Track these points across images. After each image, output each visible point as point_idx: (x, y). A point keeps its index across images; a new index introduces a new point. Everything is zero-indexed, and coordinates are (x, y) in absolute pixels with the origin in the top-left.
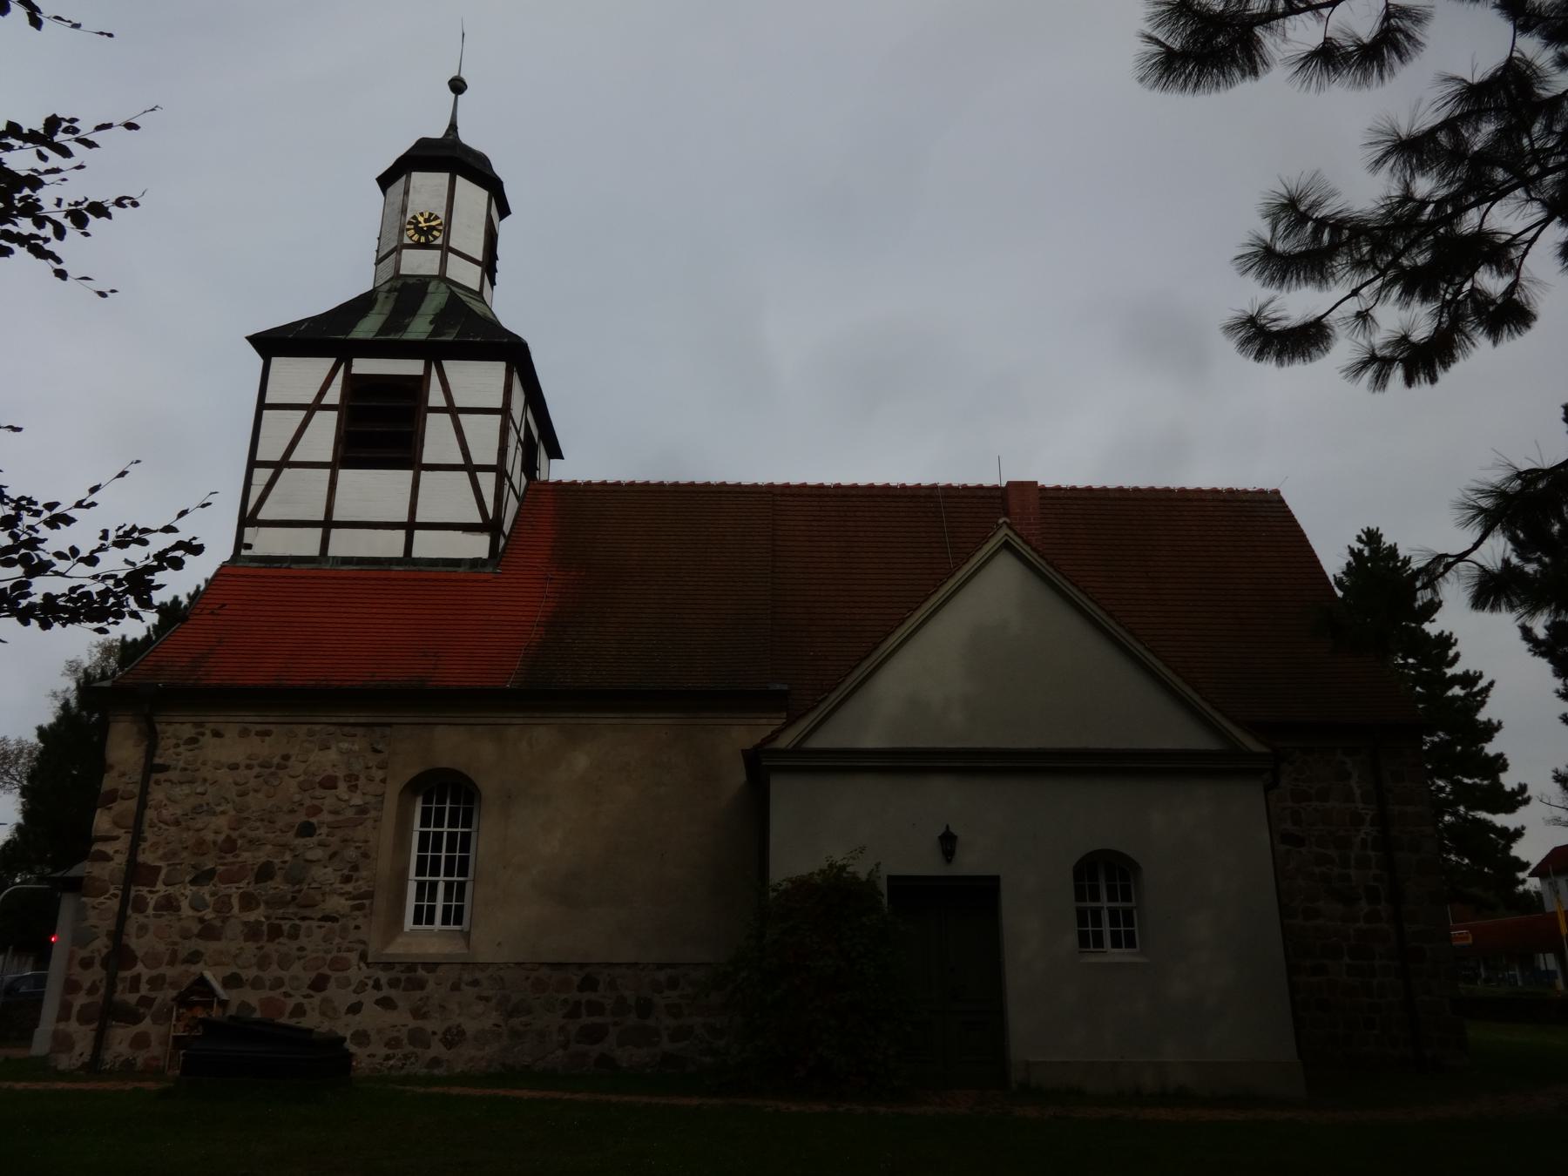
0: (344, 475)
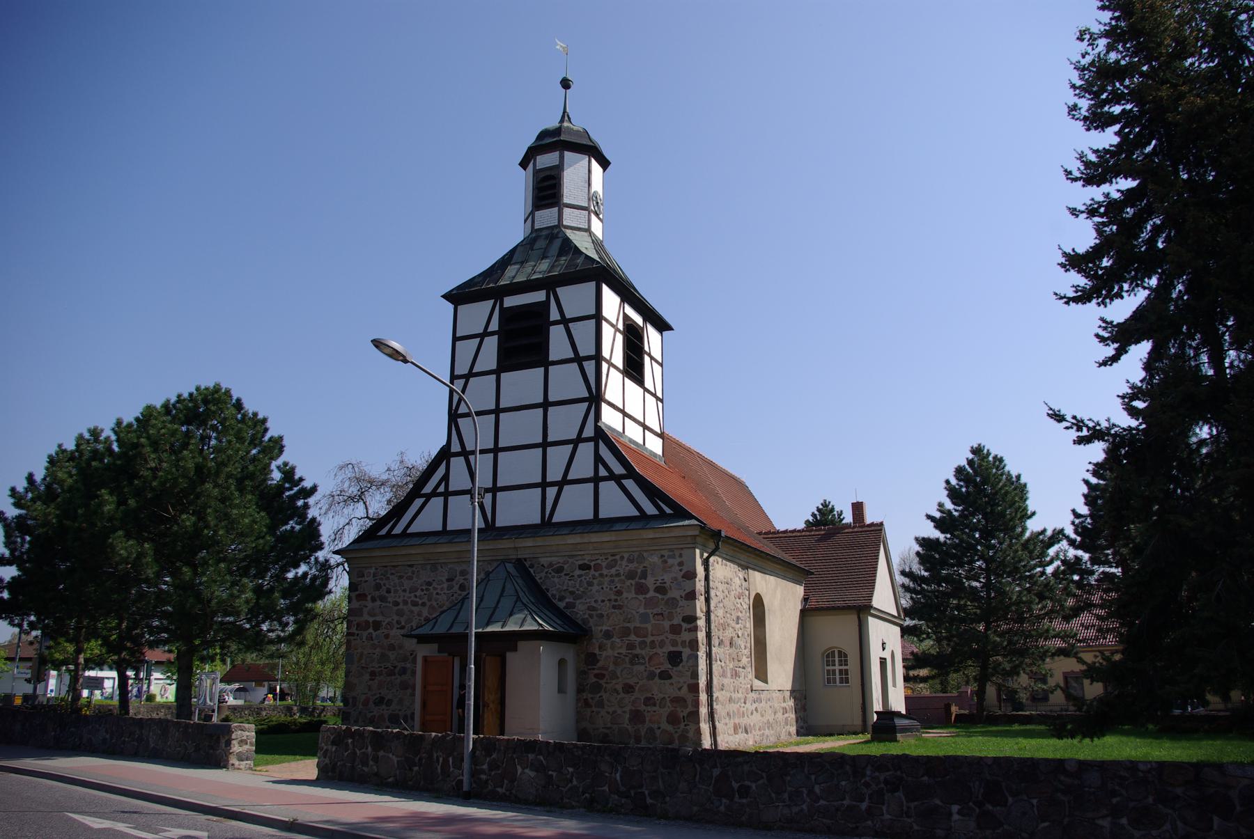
0: (505, 376)
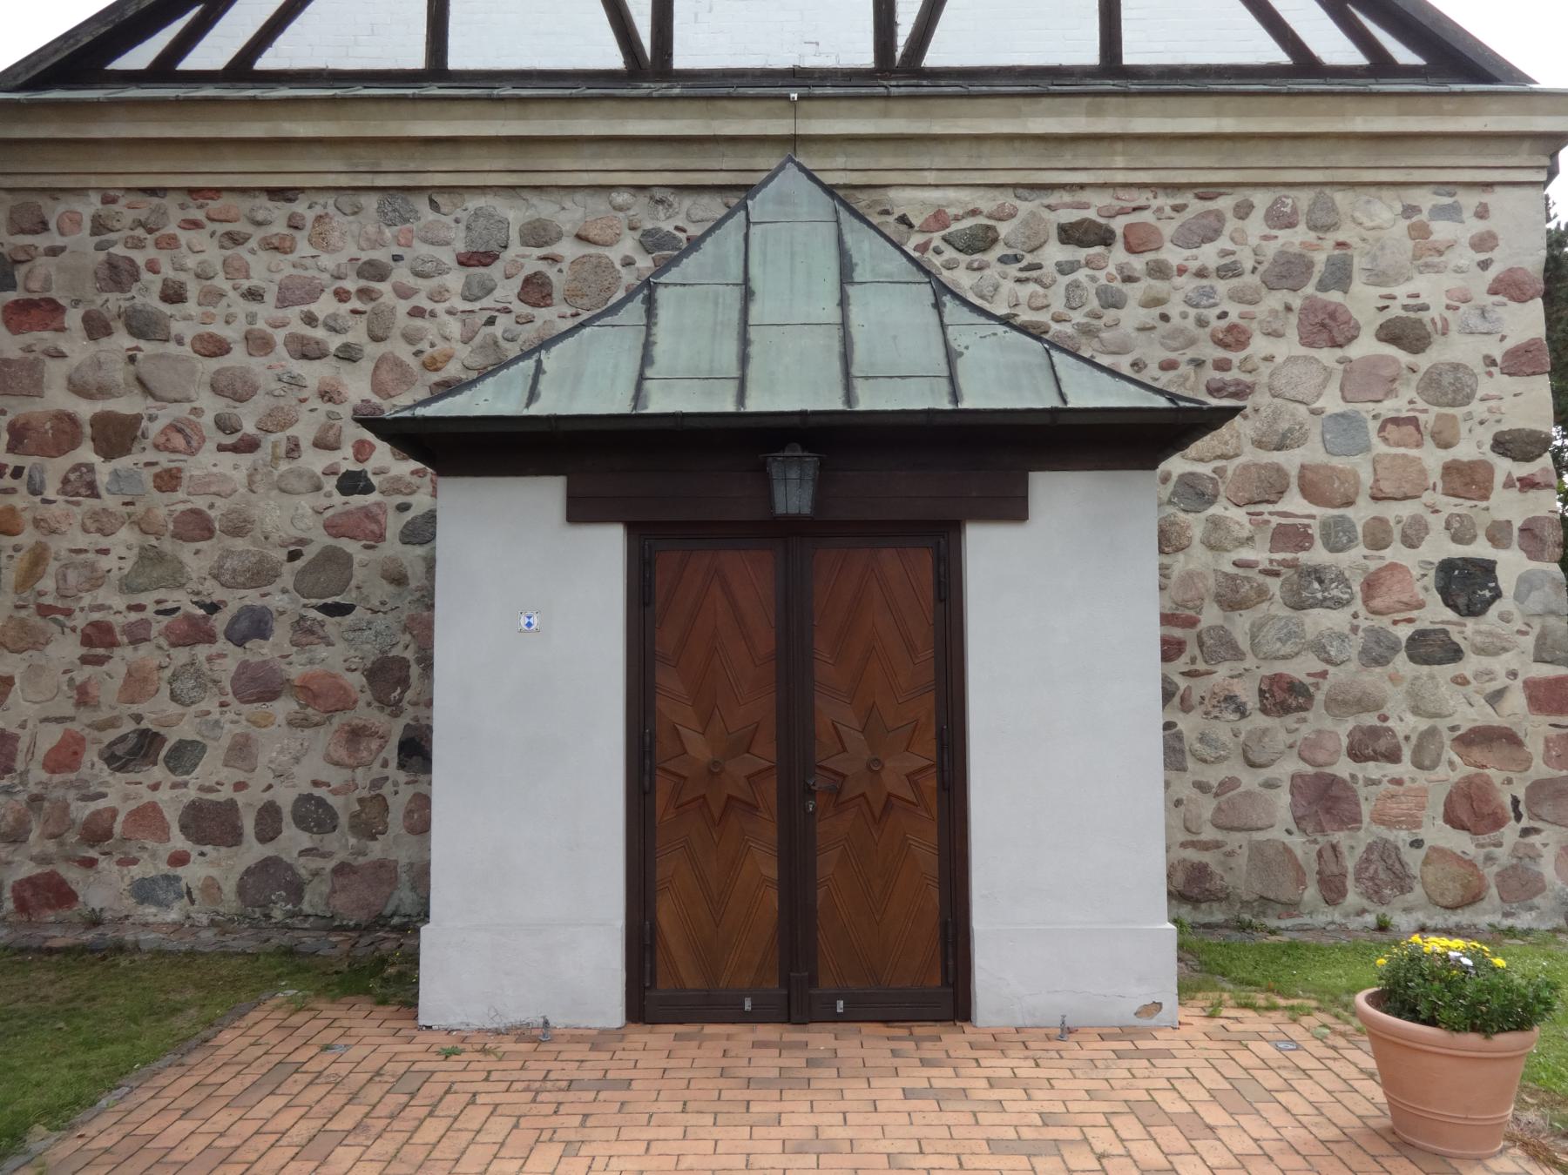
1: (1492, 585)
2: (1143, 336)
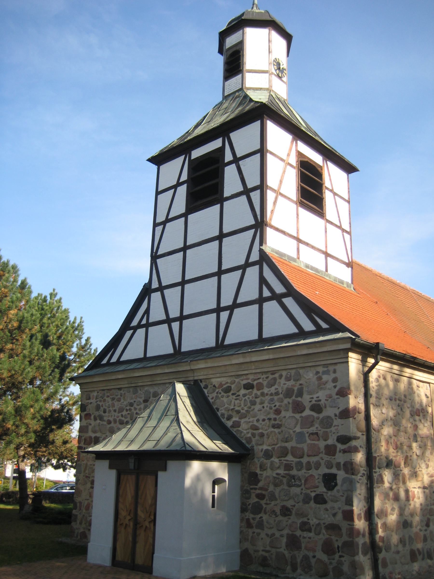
0: (190, 217)
1: (335, 481)
2: (259, 412)
